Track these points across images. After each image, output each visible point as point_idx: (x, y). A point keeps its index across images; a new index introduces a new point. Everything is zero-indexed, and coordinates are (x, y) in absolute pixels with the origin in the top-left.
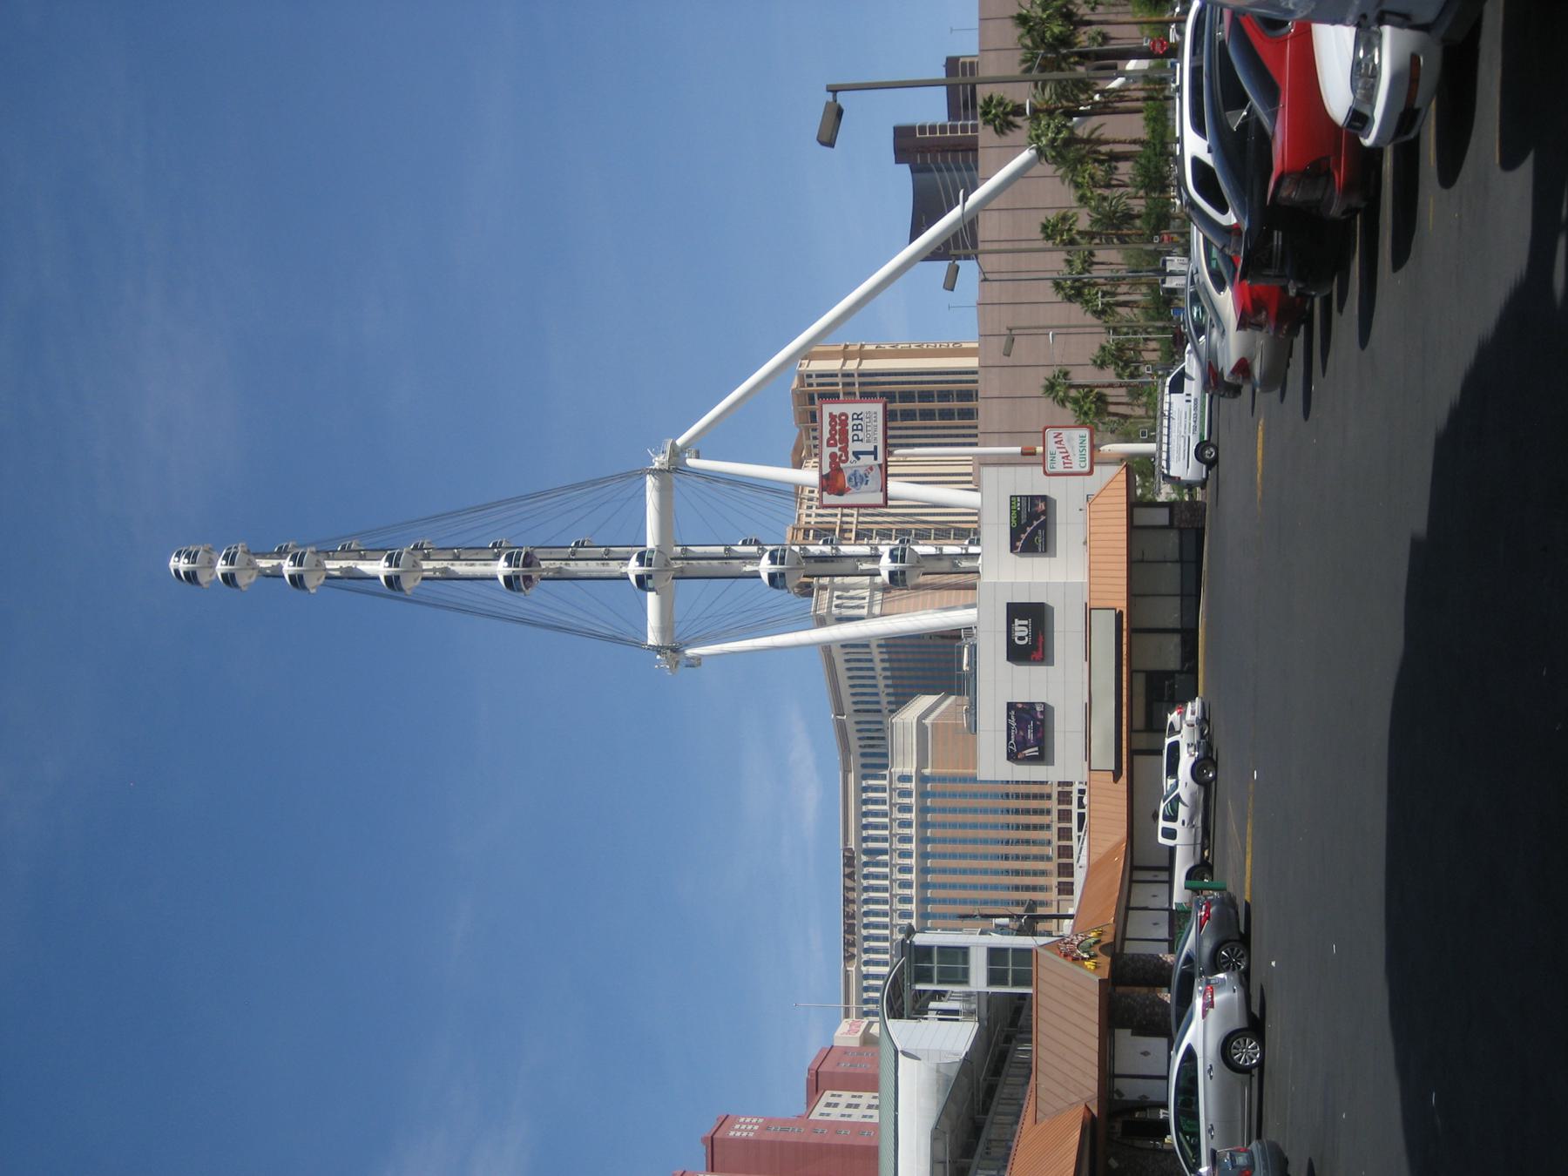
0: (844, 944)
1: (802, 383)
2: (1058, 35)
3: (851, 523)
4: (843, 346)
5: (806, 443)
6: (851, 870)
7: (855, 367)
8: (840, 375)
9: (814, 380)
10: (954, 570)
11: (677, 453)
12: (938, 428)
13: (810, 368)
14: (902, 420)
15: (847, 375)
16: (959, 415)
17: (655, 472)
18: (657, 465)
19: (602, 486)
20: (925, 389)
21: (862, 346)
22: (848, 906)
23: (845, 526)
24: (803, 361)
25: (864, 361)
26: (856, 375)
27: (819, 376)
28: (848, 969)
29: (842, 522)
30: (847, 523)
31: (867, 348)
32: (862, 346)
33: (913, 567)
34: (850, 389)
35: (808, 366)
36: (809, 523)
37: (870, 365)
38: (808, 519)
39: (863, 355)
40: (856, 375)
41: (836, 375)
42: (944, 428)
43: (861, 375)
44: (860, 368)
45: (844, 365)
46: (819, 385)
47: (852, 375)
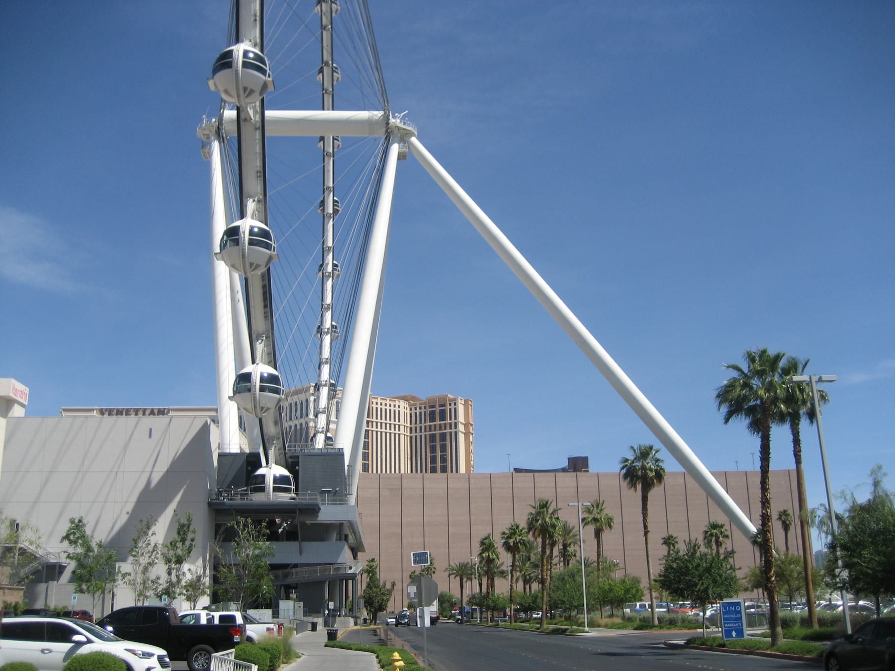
0: (110, 409)
1: (450, 400)
2: (519, 593)
3: (372, 427)
4: (473, 423)
5: (418, 403)
6: (156, 413)
7: (460, 430)
8: (455, 421)
9: (453, 406)
10: (254, 337)
11: (404, 137)
12: (426, 455)
13: (459, 404)
14: (430, 456)
15: (456, 424)
16: (433, 467)
17: (386, 118)
18: (392, 121)
19: (373, 67)
20: (447, 448)
21: (472, 434)
22: (133, 411)
23: (370, 424)
24: (463, 401)
25: (463, 435)
26: (456, 430)
27: (455, 409)
28: (95, 411)
29: (372, 422)
30: (372, 425)
31: (471, 437)
32: (472, 434)
33: (243, 256)
34: (448, 426)
35: (461, 403)
36: (373, 404)
37: (461, 438)
38: (374, 403)
39: (467, 434)
40: (456, 430)
41: (455, 419)
42: (426, 459)
43: (456, 433)
44: (460, 432)
45: (462, 423)
46: (450, 409)
47: (456, 428)
